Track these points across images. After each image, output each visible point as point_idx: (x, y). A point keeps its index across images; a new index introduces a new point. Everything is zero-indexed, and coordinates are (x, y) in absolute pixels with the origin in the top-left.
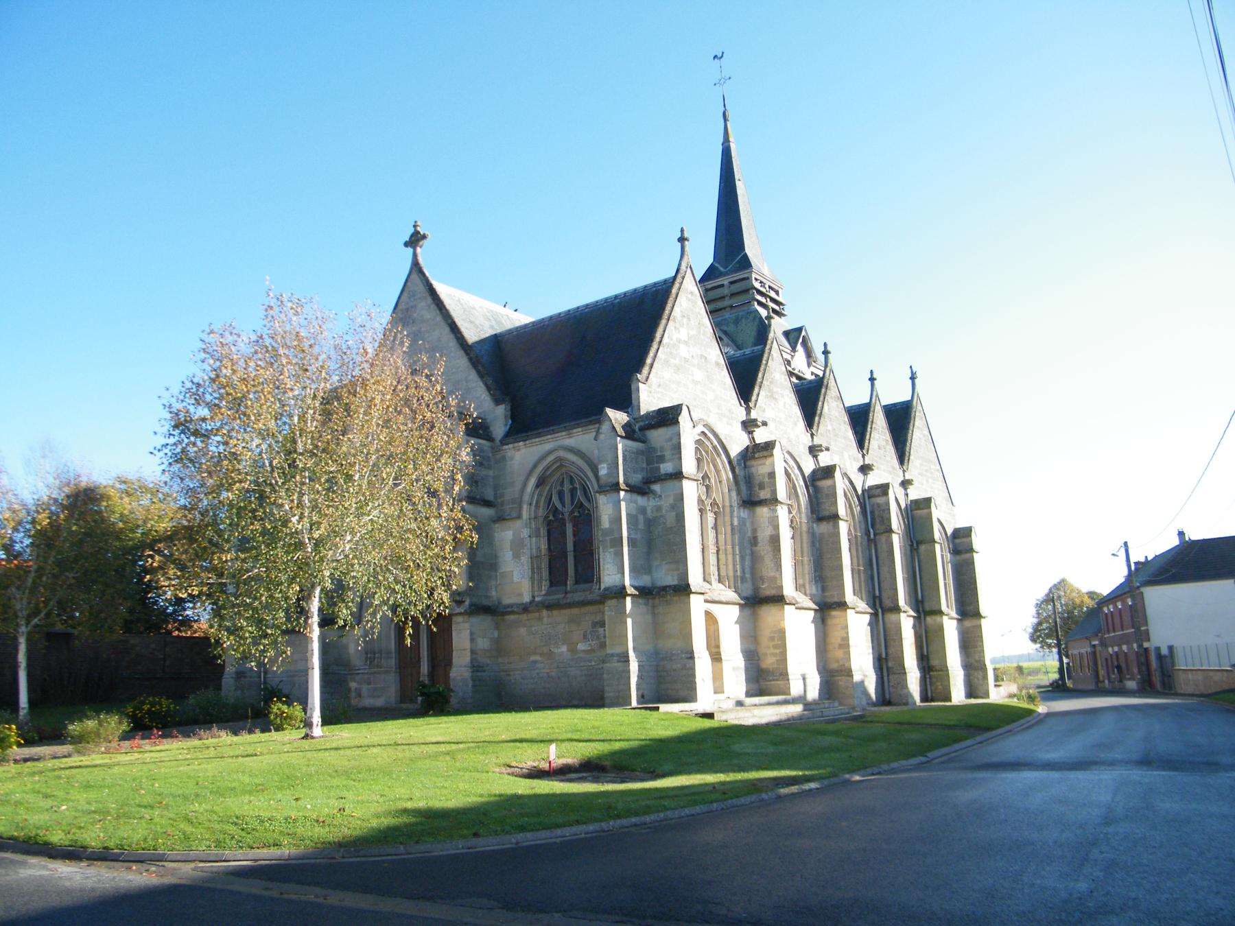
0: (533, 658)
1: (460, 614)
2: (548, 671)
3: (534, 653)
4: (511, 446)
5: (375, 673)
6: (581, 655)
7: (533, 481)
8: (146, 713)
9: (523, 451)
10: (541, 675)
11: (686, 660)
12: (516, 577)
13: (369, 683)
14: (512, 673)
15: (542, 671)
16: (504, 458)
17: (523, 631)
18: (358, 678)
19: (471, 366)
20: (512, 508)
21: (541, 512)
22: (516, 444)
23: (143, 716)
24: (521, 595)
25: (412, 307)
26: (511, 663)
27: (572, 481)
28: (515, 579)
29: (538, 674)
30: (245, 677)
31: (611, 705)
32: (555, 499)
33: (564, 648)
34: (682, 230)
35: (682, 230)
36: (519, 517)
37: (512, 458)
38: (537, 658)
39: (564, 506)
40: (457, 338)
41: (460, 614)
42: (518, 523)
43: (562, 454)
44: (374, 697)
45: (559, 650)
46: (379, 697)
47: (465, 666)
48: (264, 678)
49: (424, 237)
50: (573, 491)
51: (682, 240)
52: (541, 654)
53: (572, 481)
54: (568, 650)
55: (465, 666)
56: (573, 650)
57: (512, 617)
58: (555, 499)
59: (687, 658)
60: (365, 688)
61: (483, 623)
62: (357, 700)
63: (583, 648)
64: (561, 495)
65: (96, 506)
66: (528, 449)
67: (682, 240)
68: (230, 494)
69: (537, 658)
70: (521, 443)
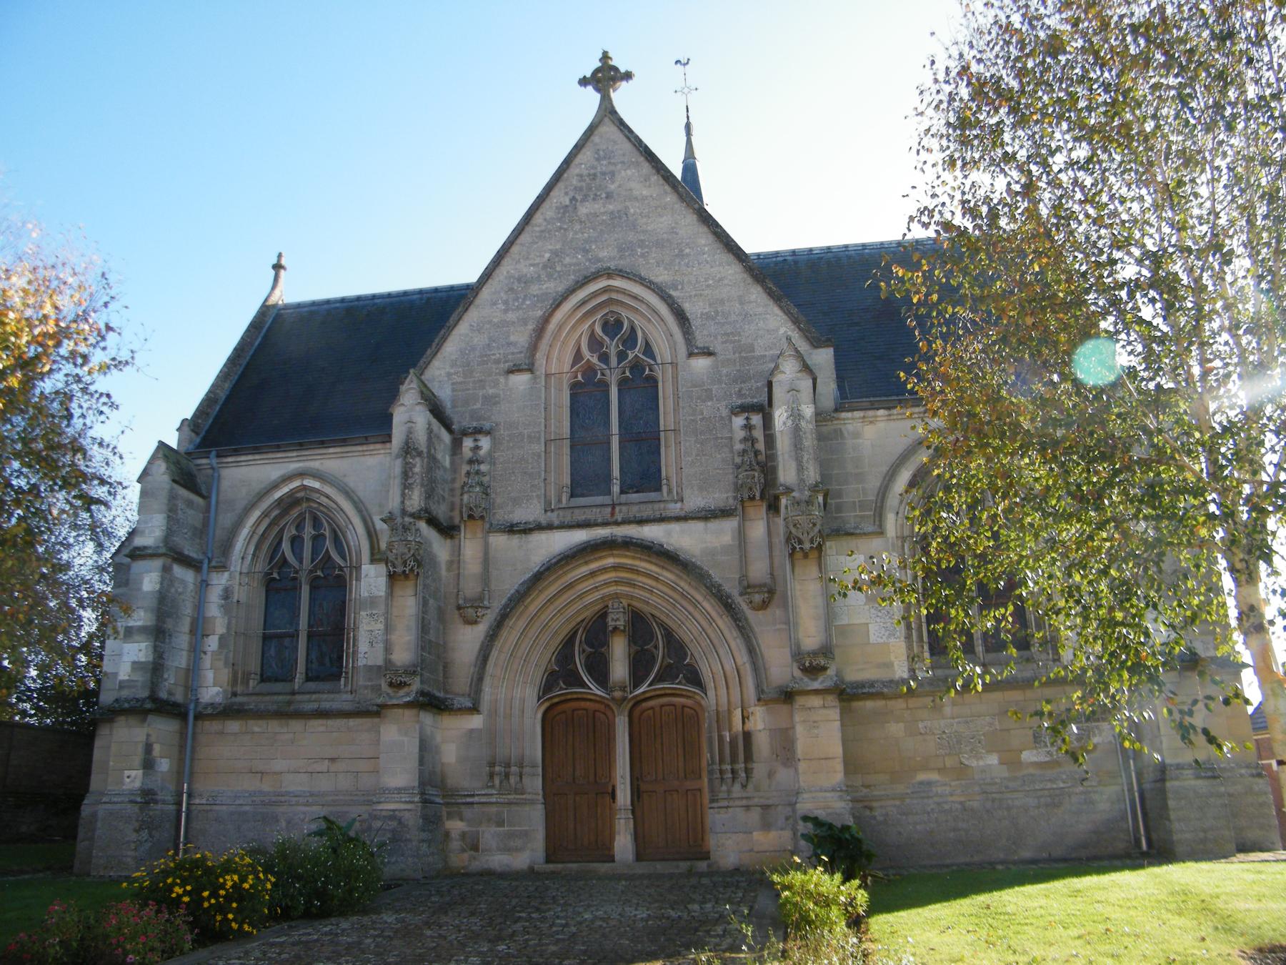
0: (921, 777)
1: (817, 692)
2: (962, 799)
3: (925, 768)
4: (858, 414)
5: (510, 804)
6: (1032, 770)
7: (904, 477)
8: (228, 898)
9: (881, 425)
10: (946, 807)
11: (1250, 779)
12: (876, 634)
13: (500, 823)
14: (875, 804)
15: (950, 799)
16: (839, 434)
17: (896, 729)
18: (467, 812)
19: (749, 280)
20: (862, 517)
21: (261, 566)
22: (871, 413)
23: (221, 909)
24: (889, 665)
25: (604, 174)
26: (868, 787)
27: (316, 523)
28: (873, 639)
29: (939, 804)
30: (156, 802)
31: (1183, 859)
32: (286, 546)
33: (993, 760)
34: (280, 256)
35: (280, 256)
36: (881, 532)
37: (857, 435)
38: (934, 776)
39: (301, 561)
40: (715, 234)
41: (817, 692)
42: (876, 543)
43: (310, 482)
44: (509, 850)
45: (981, 763)
46: (517, 850)
47: (833, 790)
48: (188, 804)
49: (584, 82)
50: (318, 539)
51: (278, 267)
52: (941, 770)
53: (316, 523)
54: (1001, 763)
55: (833, 790)
56: (1011, 761)
57: (869, 704)
58: (286, 546)
59: (1253, 776)
60: (489, 835)
61: (162, 729)
62: (466, 856)
63: (1035, 759)
64: (296, 541)
65: (31, 371)
66: (892, 424)
67: (278, 267)
68: (980, 346)
69: (934, 776)
70: (881, 412)
